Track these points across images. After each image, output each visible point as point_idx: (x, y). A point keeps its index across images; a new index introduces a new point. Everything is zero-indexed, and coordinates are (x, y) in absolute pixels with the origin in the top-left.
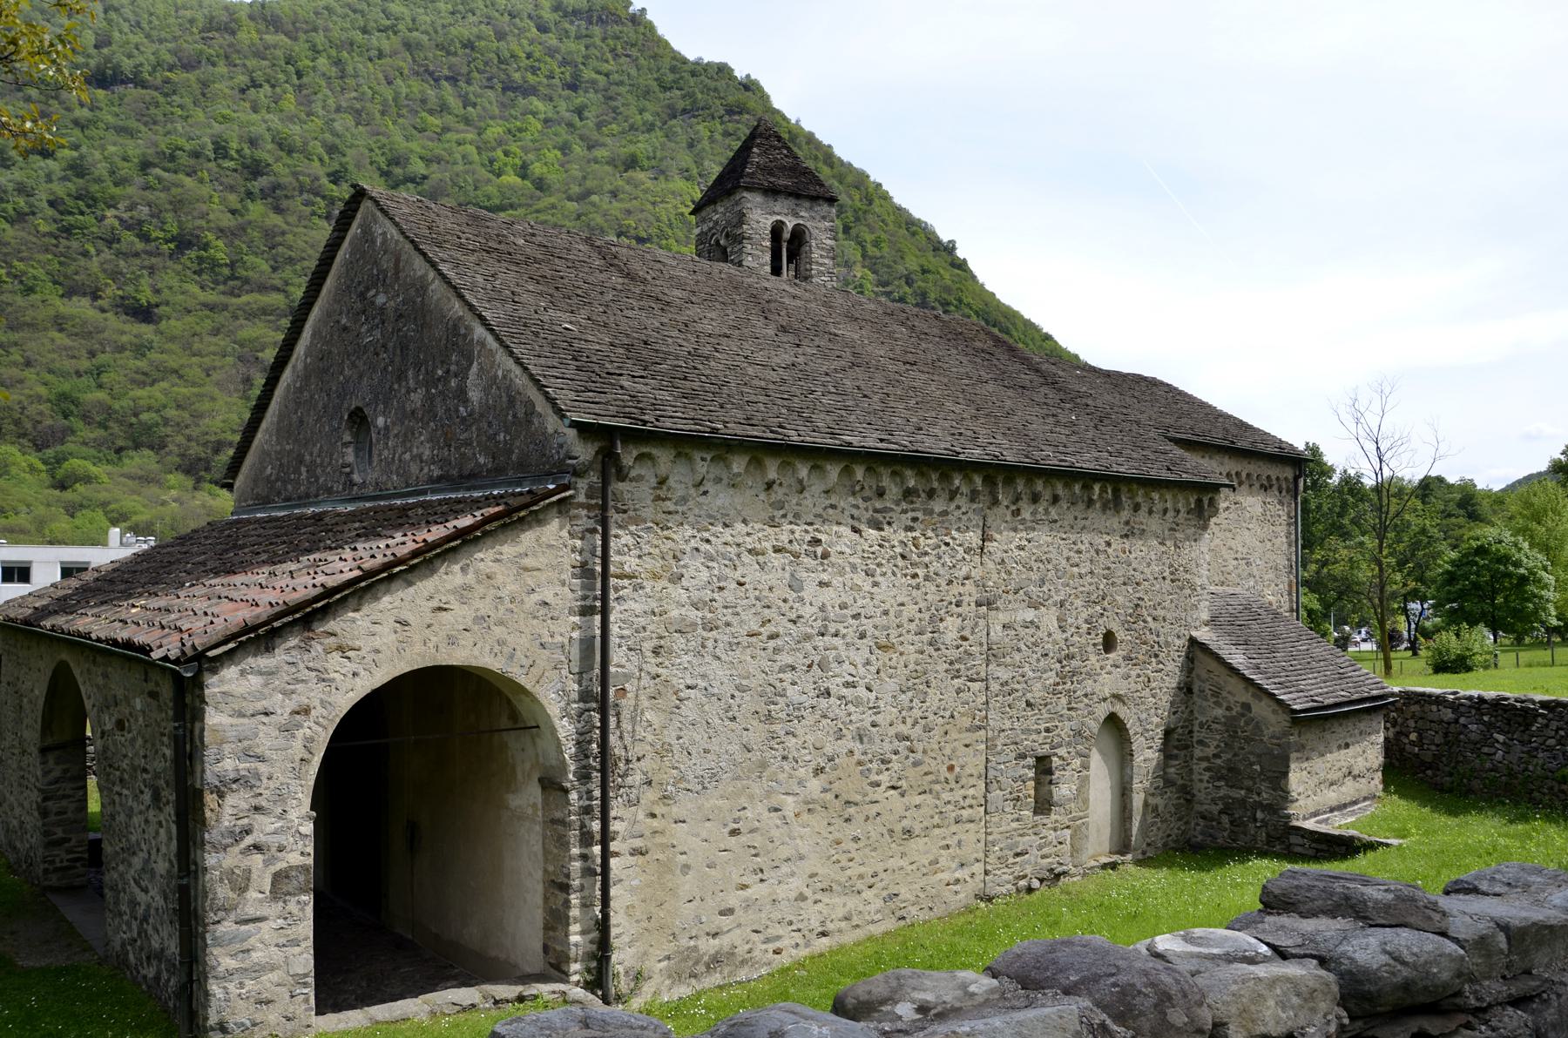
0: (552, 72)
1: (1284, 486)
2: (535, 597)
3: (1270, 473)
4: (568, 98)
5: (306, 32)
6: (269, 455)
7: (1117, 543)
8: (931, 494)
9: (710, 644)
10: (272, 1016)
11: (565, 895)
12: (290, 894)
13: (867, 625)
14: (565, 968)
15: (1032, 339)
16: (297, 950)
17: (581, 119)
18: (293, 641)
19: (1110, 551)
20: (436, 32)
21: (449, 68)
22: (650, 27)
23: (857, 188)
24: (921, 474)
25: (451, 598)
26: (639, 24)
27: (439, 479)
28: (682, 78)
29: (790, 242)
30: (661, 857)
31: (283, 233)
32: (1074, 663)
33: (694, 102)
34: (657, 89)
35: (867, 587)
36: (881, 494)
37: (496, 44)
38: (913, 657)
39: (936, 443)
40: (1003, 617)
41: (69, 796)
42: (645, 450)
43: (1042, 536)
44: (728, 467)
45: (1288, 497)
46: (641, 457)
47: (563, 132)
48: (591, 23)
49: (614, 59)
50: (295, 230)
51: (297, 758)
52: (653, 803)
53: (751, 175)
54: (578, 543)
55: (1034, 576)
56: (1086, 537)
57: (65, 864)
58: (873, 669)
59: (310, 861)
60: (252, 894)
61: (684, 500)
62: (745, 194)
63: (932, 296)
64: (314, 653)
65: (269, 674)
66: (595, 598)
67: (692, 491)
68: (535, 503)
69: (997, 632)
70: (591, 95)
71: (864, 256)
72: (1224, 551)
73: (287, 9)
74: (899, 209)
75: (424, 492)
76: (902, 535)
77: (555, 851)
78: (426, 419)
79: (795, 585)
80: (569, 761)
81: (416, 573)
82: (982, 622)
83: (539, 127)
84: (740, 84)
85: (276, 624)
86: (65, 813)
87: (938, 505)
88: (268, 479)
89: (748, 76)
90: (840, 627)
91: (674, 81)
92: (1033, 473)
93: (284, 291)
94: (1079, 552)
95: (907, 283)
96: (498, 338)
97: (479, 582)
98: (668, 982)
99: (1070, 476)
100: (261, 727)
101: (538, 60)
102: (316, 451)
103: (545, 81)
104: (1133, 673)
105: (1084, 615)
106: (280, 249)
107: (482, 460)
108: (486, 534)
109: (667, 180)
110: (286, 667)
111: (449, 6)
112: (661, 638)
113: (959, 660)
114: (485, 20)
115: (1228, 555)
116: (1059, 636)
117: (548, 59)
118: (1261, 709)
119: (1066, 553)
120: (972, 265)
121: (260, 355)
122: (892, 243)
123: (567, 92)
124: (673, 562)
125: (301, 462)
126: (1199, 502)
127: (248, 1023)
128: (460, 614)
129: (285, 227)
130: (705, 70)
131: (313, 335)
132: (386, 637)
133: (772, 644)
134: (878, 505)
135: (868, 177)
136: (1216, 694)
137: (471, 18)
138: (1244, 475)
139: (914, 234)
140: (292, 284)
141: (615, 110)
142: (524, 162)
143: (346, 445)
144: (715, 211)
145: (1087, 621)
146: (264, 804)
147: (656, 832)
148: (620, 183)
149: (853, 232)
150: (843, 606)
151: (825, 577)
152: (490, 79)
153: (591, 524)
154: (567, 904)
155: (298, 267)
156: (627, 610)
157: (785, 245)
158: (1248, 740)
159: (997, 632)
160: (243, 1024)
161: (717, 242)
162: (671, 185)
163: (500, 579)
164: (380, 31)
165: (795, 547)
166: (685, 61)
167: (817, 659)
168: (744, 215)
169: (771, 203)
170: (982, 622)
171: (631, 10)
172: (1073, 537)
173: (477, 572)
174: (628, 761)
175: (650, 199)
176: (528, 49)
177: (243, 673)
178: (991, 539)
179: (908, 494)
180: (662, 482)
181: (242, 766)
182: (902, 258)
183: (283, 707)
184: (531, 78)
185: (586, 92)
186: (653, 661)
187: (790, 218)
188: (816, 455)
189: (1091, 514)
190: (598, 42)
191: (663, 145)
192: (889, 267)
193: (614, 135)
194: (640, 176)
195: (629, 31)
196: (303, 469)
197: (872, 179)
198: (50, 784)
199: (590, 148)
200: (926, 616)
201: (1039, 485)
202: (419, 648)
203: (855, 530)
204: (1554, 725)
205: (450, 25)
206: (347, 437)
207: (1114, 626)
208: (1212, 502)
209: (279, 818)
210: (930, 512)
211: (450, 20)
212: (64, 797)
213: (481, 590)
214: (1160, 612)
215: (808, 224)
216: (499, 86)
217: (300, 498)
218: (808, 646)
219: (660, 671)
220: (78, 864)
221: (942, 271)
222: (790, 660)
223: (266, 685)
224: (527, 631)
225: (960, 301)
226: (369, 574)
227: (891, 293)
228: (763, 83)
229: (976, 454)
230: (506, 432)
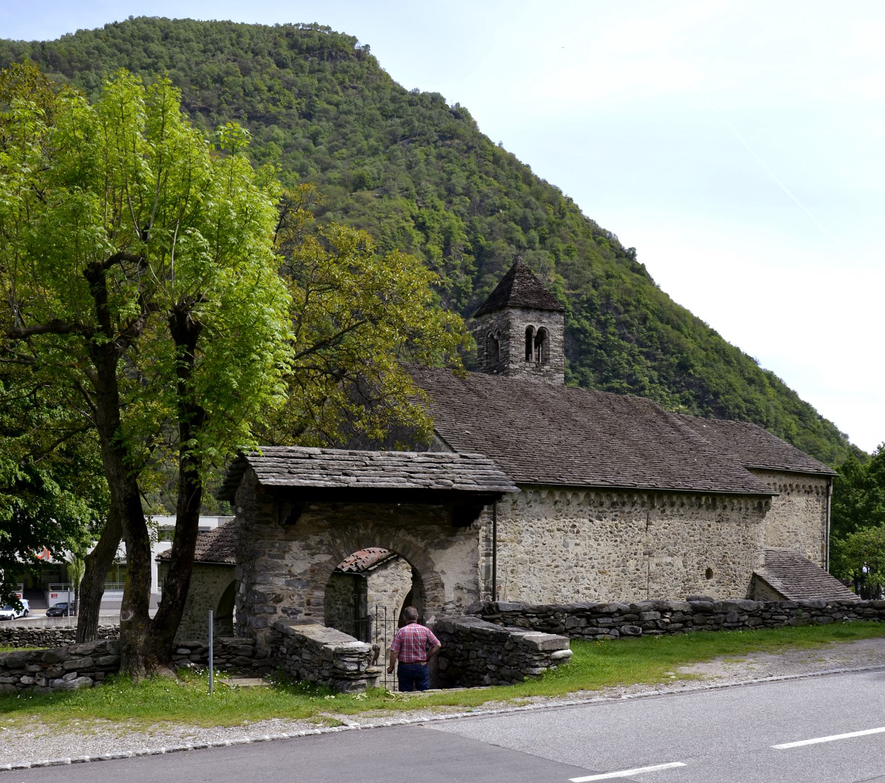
0: (290, 103)
1: (820, 490)
3: (811, 484)
4: (304, 126)
5: (80, 70)
7: (714, 525)
8: (624, 504)
9: (532, 569)
13: (595, 563)
15: (700, 335)
17: (316, 144)
18: (393, 565)
19: (710, 529)
20: (190, 69)
21: (203, 101)
22: (373, 62)
23: (552, 203)
24: (619, 495)
26: (364, 59)
28: (401, 107)
29: (536, 338)
32: (690, 583)
33: (412, 130)
34: (380, 117)
35: (595, 546)
36: (601, 504)
37: (241, 79)
38: (615, 577)
39: (626, 481)
40: (656, 560)
43: (676, 522)
44: (540, 495)
45: (823, 497)
47: (301, 156)
48: (322, 59)
49: (343, 91)
55: (671, 541)
56: (698, 522)
58: (597, 582)
61: (523, 509)
63: (615, 298)
69: (653, 567)
70: (324, 123)
71: (557, 262)
72: (781, 528)
73: (63, 50)
74: (587, 221)
76: (610, 523)
79: (565, 545)
82: (646, 563)
83: (280, 152)
84: (451, 112)
87: (627, 509)
89: (458, 105)
90: (584, 563)
91: (394, 111)
92: (671, 493)
94: (694, 530)
95: (594, 286)
96: (441, 438)
99: (690, 494)
101: (278, 93)
103: (284, 111)
104: (722, 590)
105: (696, 560)
109: (390, 198)
111: (201, 45)
113: (635, 580)
114: (232, 58)
115: (784, 530)
116: (683, 570)
117: (286, 92)
119: (687, 530)
120: (649, 270)
122: (581, 252)
123: (303, 121)
126: (760, 504)
133: (556, 570)
134: (600, 510)
135: (561, 192)
137: (220, 56)
138: (794, 486)
139: (599, 243)
141: (344, 136)
145: (697, 563)
148: (351, 201)
149: (548, 242)
150: (585, 554)
151: (578, 542)
152: (237, 110)
153: (488, 520)
156: (503, 553)
157: (533, 340)
159: (653, 567)
161: (492, 336)
162: (393, 203)
164: (142, 68)
165: (566, 528)
166: (403, 92)
167: (574, 577)
169: (526, 315)
170: (646, 563)
171: (357, 46)
172: (691, 522)
175: (376, 215)
176: (269, 83)
177: (378, 576)
178: (651, 524)
179: (613, 504)
180: (515, 502)
182: (590, 265)
184: (272, 108)
185: (319, 120)
188: (575, 489)
189: (701, 511)
190: (329, 76)
191: (386, 169)
192: (578, 272)
193: (344, 159)
194: (367, 194)
195: (355, 64)
197: (564, 194)
199: (324, 170)
200: (621, 559)
201: (675, 499)
203: (590, 521)
205: (202, 62)
207: (712, 566)
208: (767, 504)
210: (623, 512)
211: (202, 58)
214: (737, 560)
215: (548, 327)
216: (245, 116)
218: (570, 571)
221: (624, 276)
222: (562, 577)
225: (639, 302)
227: (579, 295)
228: (470, 111)
229: (644, 485)
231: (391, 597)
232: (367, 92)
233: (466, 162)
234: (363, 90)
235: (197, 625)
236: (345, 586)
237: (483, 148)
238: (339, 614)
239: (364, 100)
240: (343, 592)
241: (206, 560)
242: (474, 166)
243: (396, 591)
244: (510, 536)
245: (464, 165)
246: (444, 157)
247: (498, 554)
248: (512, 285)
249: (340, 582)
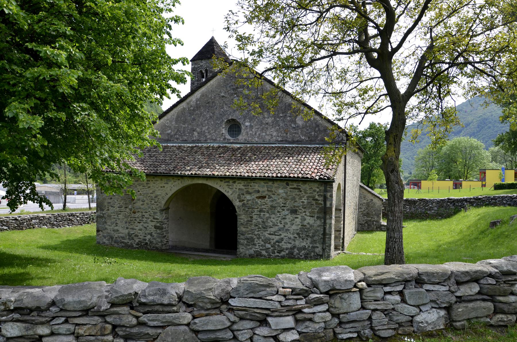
107: (303, 138)
118: (376, 200)
131: (202, 95)
136: (364, 197)
143: (223, 128)
158: (372, 207)
204: (422, 203)
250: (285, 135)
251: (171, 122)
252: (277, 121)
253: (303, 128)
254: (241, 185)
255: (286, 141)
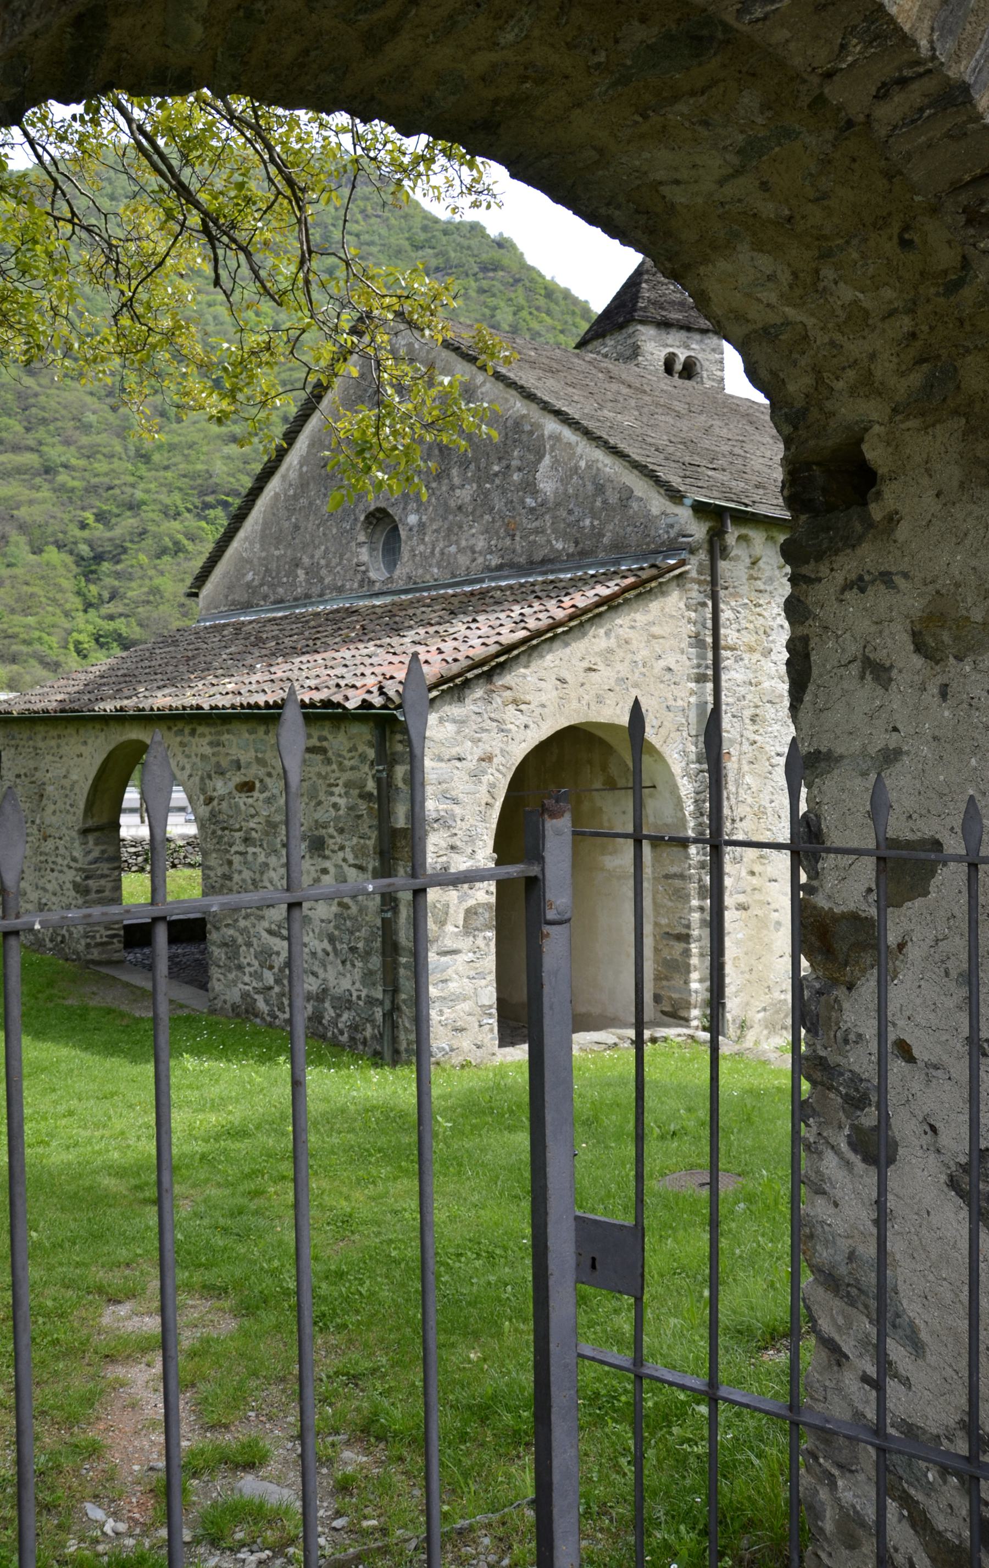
2: (662, 663)
6: (249, 561)
10: (465, 1043)
11: (683, 945)
12: (477, 929)
14: (683, 1013)
16: (483, 982)
18: (479, 692)
25: (598, 660)
27: (500, 567)
28: (434, 237)
30: (760, 913)
31: (36, 395)
33: (448, 260)
34: (409, 248)
41: (107, 876)
42: (744, 531)
46: (740, 538)
49: (364, 220)
50: (49, 391)
51: (483, 802)
52: (753, 861)
53: (644, 309)
54: (693, 615)
57: (105, 939)
59: (493, 899)
60: (450, 928)
62: (639, 327)
64: (495, 705)
65: (461, 722)
66: (707, 667)
67: (777, 572)
68: (661, 576)
75: (481, 581)
77: (670, 904)
78: (478, 513)
80: (689, 818)
81: (571, 635)
84: (493, 241)
85: (469, 675)
86: (103, 891)
88: (249, 585)
89: (501, 234)
91: (426, 240)
93: (38, 451)
97: (619, 646)
98: (765, 1032)
100: (455, 771)
102: (318, 553)
106: (34, 410)
107: (559, 546)
108: (627, 601)
110: (474, 717)
112: (757, 707)
121: (15, 512)
124: (763, 636)
125: (297, 565)
127: (447, 1048)
128: (605, 676)
129: (37, 389)
130: (458, 229)
132: (550, 694)
140: (46, 444)
142: (276, 322)
143: (360, 545)
144: (605, 345)
146: (459, 843)
147: (754, 889)
153: (701, 598)
154: (687, 953)
155: (51, 428)
160: (443, 1049)
163: (635, 645)
168: (639, 347)
169: (664, 336)
173: (617, 637)
174: (733, 821)
177: (441, 720)
181: (441, 807)
183: (472, 753)
186: (751, 728)
187: (682, 350)
196: (300, 572)
198: (90, 863)
202: (575, 704)
206: (362, 538)
209: (470, 858)
212: (103, 876)
213: (620, 653)
215: (699, 356)
217: (296, 599)
219: (757, 738)
220: (115, 940)
223: (458, 732)
224: (656, 694)
226: (538, 633)
230: (594, 517)
231: (475, 776)
232: (393, 221)
233: (513, 295)
234: (388, 219)
235: (50, 844)
236: (353, 749)
237: (532, 280)
238: (337, 819)
239: (390, 229)
240: (348, 763)
241: (62, 711)
242: (522, 301)
243: (487, 758)
244: (748, 638)
245: (510, 300)
246: (485, 291)
247: (724, 677)
248: (638, 291)
249: (341, 737)
250: (508, 542)
251: (252, 543)
252: (486, 494)
253: (558, 505)
254: (205, 741)
255: (512, 565)
